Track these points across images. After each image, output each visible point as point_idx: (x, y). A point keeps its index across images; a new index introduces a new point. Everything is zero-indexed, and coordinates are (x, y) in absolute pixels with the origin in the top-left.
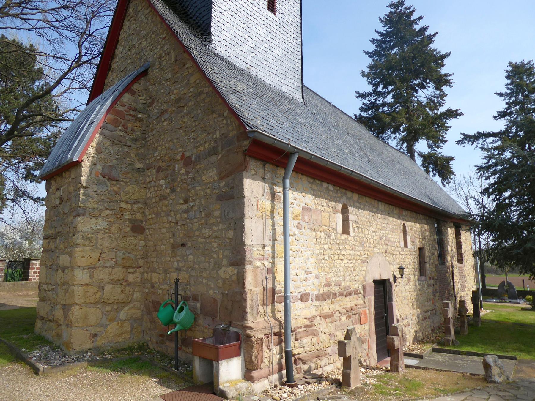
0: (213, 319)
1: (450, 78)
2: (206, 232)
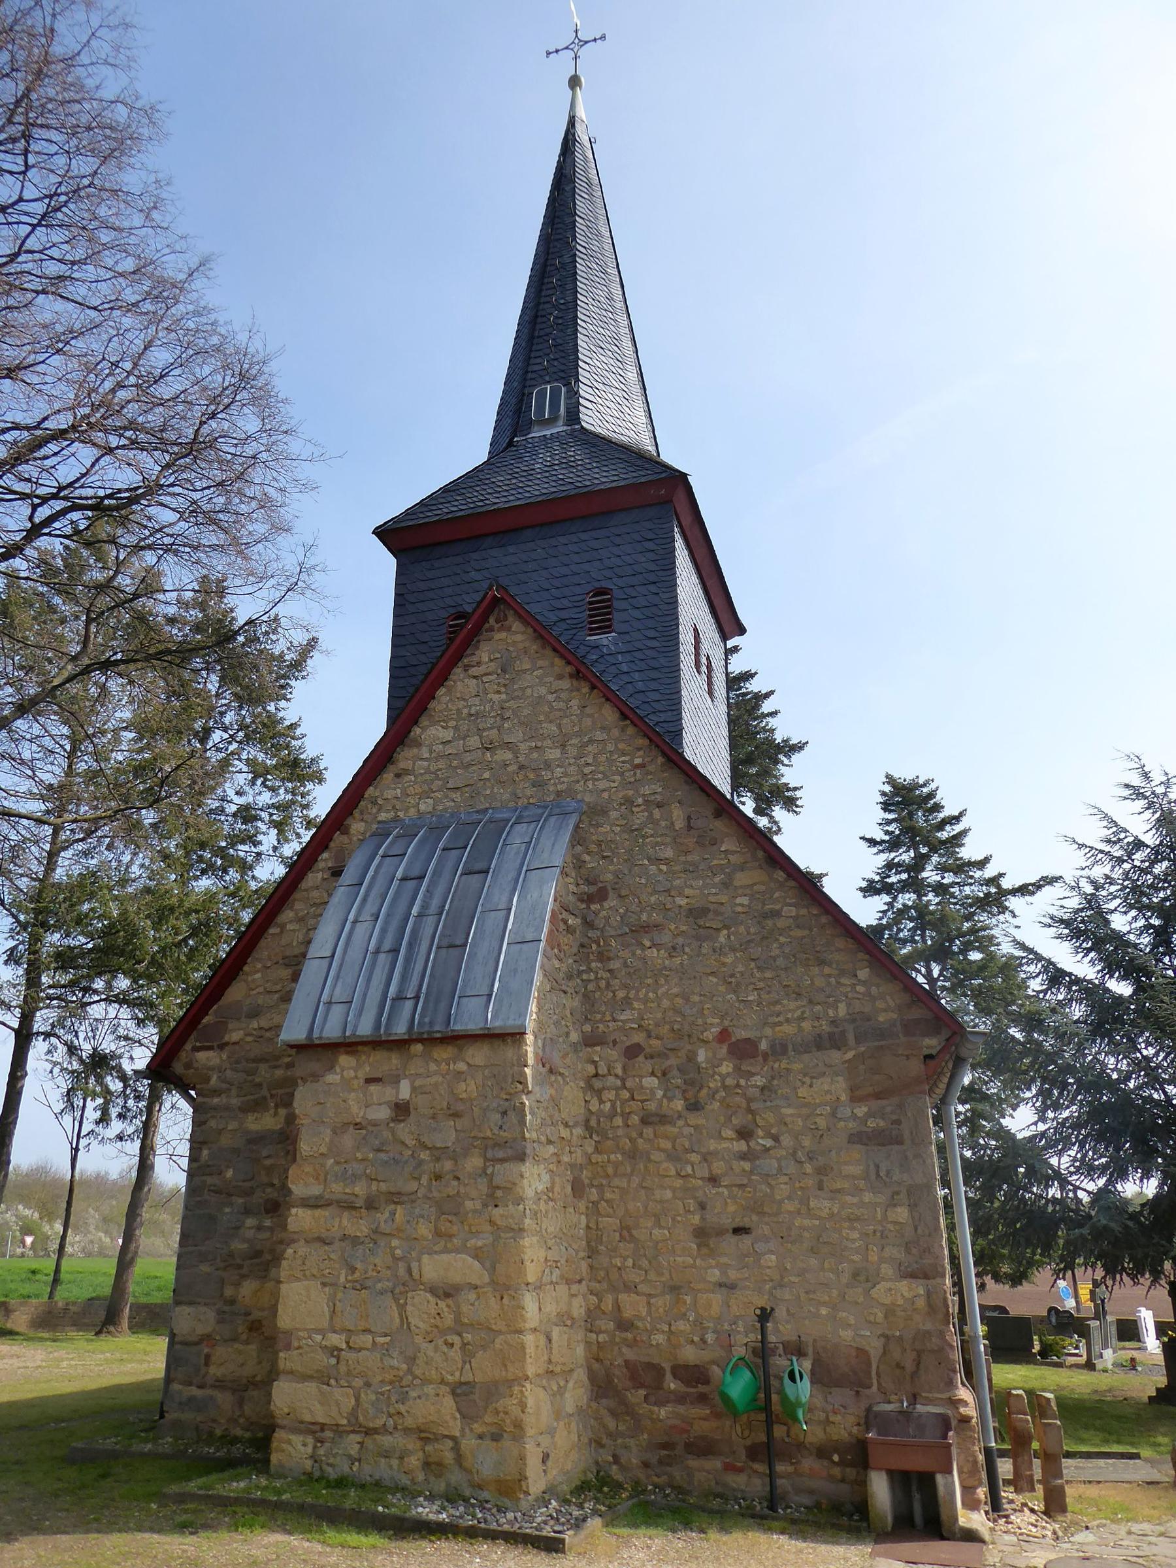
0: (858, 1392)
1: (798, 794)
2: (823, 1205)
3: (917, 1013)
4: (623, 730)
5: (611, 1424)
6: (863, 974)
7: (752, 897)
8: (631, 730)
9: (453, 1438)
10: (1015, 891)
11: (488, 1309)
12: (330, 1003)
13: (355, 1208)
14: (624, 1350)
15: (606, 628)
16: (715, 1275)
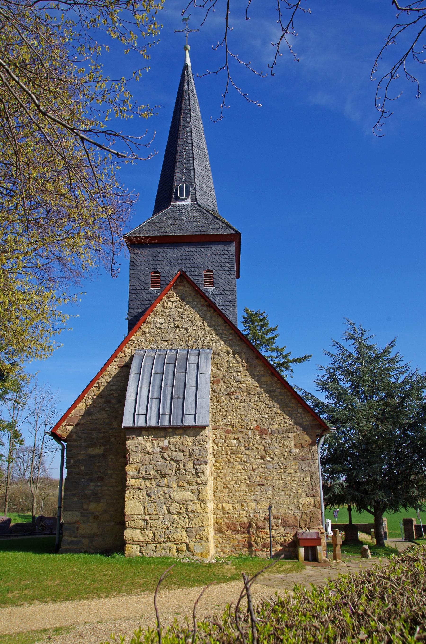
3: (315, 422)
4: (225, 327)
5: (221, 540)
6: (300, 410)
7: (267, 385)
8: (228, 327)
9: (186, 543)
10: (295, 361)
11: (197, 507)
12: (138, 415)
13: (150, 479)
14: (225, 519)
15: (212, 284)
16: (253, 497)
